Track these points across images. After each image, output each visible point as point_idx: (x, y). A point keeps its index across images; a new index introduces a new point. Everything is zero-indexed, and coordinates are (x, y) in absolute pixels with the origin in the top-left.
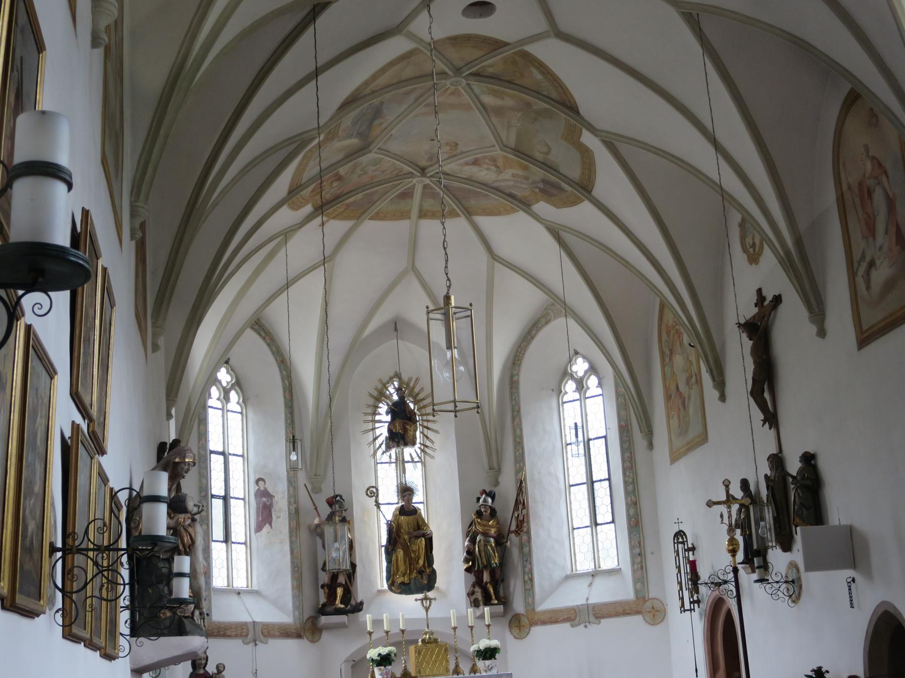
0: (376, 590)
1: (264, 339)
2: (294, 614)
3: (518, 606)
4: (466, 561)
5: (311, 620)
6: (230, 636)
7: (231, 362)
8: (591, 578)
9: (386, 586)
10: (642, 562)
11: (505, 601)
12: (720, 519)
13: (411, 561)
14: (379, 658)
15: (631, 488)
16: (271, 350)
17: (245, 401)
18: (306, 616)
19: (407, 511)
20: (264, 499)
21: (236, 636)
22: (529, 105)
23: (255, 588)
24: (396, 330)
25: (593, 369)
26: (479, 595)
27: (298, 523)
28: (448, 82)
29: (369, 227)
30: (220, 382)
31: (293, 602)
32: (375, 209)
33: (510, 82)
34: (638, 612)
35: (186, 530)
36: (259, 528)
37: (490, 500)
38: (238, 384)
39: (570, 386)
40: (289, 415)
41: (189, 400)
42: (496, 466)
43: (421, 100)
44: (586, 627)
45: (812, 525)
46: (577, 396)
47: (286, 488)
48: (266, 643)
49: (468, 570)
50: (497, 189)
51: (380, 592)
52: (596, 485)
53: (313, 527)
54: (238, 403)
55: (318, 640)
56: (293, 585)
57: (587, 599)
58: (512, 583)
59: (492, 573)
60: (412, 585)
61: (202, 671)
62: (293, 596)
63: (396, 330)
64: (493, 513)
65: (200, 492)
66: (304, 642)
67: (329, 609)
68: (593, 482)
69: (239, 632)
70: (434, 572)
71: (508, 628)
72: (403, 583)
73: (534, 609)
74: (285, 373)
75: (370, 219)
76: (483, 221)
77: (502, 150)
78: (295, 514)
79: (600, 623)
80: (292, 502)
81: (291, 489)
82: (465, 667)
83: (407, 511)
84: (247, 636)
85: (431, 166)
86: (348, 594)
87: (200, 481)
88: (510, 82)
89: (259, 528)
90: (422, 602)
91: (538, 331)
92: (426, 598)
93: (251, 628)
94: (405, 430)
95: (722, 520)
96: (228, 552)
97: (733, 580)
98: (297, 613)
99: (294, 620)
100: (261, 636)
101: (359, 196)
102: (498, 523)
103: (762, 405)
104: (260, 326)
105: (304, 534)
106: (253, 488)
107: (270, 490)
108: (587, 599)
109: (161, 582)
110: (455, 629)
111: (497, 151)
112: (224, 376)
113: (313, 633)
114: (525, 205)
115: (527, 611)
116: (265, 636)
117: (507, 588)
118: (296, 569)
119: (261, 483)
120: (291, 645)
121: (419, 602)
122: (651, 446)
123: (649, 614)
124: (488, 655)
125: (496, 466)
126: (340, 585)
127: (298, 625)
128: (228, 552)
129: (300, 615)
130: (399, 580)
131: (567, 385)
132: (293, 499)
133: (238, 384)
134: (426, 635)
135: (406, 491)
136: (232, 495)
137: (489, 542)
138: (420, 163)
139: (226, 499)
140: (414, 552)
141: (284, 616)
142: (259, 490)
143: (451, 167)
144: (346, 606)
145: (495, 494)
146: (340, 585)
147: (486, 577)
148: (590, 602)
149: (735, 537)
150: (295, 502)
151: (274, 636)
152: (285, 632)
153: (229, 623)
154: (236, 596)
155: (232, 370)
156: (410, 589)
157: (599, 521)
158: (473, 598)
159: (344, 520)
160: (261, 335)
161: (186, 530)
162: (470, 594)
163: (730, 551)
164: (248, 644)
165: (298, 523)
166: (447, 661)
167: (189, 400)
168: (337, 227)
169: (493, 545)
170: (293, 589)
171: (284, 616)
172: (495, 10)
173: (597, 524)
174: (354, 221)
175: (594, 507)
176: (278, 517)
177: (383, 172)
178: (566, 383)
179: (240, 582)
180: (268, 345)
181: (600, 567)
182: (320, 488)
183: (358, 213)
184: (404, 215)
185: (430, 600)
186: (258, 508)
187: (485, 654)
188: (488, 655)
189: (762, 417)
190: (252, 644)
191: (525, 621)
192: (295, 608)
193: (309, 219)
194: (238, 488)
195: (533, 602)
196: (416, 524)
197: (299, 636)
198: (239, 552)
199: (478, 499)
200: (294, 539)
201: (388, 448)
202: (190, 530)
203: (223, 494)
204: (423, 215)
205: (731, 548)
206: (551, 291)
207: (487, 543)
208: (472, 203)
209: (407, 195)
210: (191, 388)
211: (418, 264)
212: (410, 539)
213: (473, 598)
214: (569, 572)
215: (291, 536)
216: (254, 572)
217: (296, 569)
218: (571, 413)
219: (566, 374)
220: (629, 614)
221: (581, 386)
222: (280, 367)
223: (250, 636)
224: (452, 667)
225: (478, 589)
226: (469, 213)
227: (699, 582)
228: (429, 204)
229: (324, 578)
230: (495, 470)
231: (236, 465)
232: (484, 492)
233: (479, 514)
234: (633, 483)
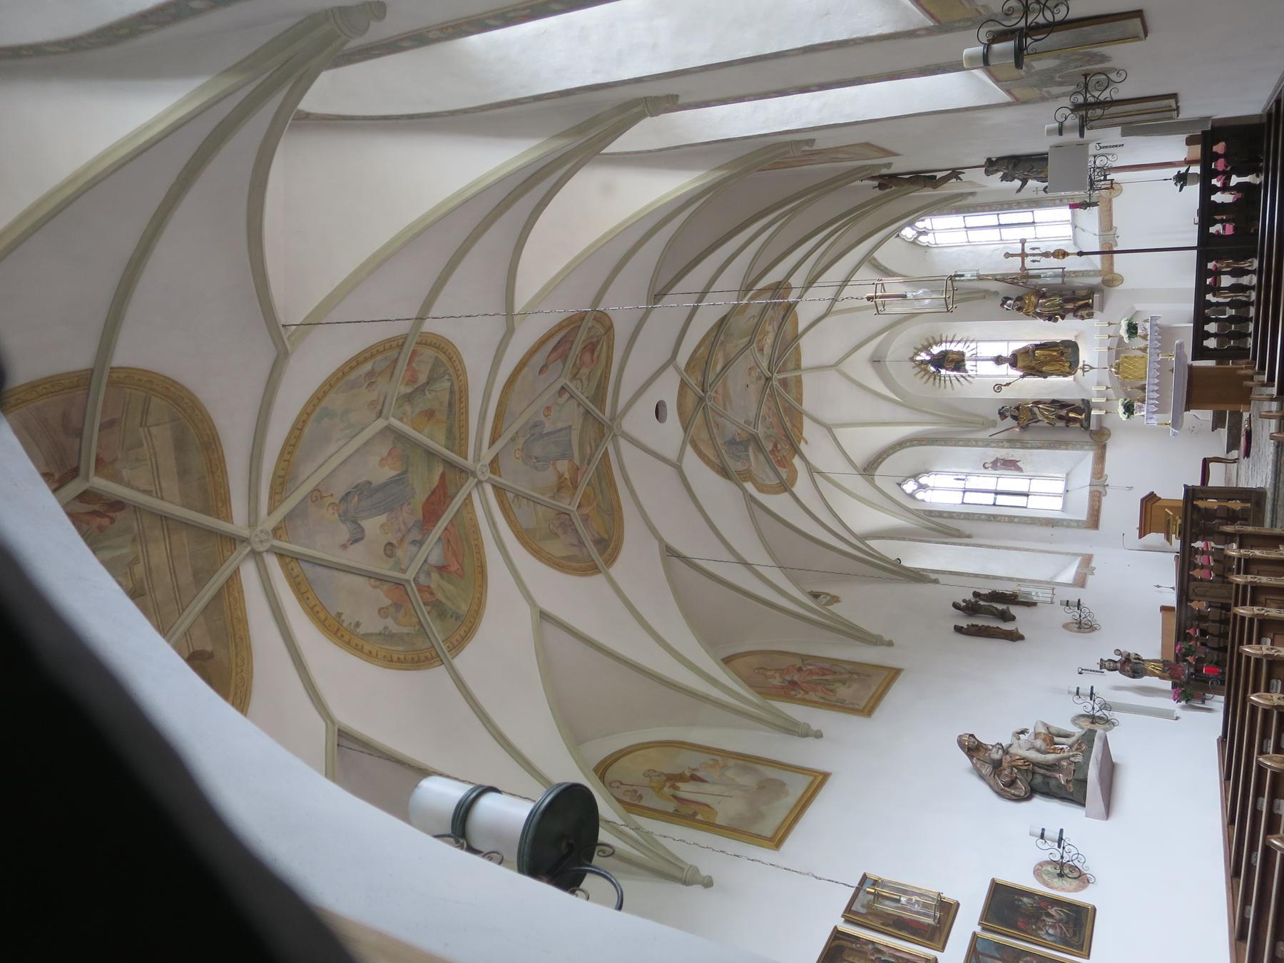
0: (1074, 383)
1: (884, 459)
2: (1086, 450)
3: (1096, 281)
4: (1056, 320)
5: (1092, 435)
6: (1099, 507)
7: (899, 482)
8: (1077, 229)
9: (1070, 378)
10: (1067, 199)
11: (1091, 291)
12: (1037, 263)
13: (1053, 360)
14: (1127, 414)
15: (1006, 206)
16: (892, 454)
17: (928, 472)
18: (1088, 439)
19: (1014, 361)
20: (999, 464)
21: (1100, 501)
22: (722, 343)
23: (1064, 476)
24: (879, 361)
25: (911, 224)
26: (1084, 313)
27: (1018, 441)
28: (709, 404)
29: (807, 405)
30: (914, 491)
31: (1077, 450)
32: (795, 404)
33: (707, 363)
34: (1110, 200)
35: (1014, 761)
36: (1020, 469)
37: (1009, 302)
38: (915, 477)
39: (923, 239)
40: (938, 443)
41: (927, 528)
42: (983, 294)
43: (721, 413)
44: (1118, 237)
45: (1047, 164)
46: (931, 235)
47: (991, 449)
48: (1107, 476)
49: (1063, 318)
50: (779, 328)
51: (1075, 380)
52: (1001, 223)
53: (1022, 430)
54: (925, 492)
55: (1109, 430)
56: (1064, 449)
57: (1095, 235)
58: (1076, 284)
59: (1067, 301)
60: (1072, 360)
61: (1119, 665)
62: (1073, 449)
63: (879, 361)
64: (1019, 299)
65: (991, 521)
66: (1110, 443)
67: (1085, 424)
68: (1000, 225)
69: (1096, 499)
70: (1063, 342)
71: (1114, 288)
72: (1070, 367)
73: (1100, 271)
74: (908, 444)
75: (801, 405)
76: (801, 328)
77: (753, 344)
78: (1013, 443)
79: (1107, 476)
80: (1001, 444)
81: (993, 445)
82: (1142, 343)
83: (1014, 361)
84: (1100, 493)
85: (764, 375)
86: (1077, 410)
87: (983, 520)
88: (707, 363)
89: (1020, 469)
90: (1086, 371)
91: (881, 265)
92: (1083, 369)
93: (1095, 488)
94: (953, 361)
95: (1038, 261)
96: (1035, 494)
97: (1091, 100)
98: (1086, 447)
99: (1092, 450)
100: (1102, 480)
101: (786, 419)
102: (1027, 294)
103: (945, 179)
104: (875, 462)
105: (1027, 436)
106: (990, 471)
107: (993, 460)
108: (1095, 235)
109: (1048, 784)
110: (1110, 324)
111: (754, 348)
112: (910, 487)
113: (1103, 435)
114: (790, 307)
115: (1101, 276)
116: (1101, 477)
117: (1081, 288)
118: (1052, 445)
119: (987, 465)
120: (1113, 454)
121: (1085, 374)
122: (972, 194)
123: (1112, 194)
124: (1134, 331)
125: (983, 294)
126: (1067, 414)
127: (1095, 447)
128: (1035, 494)
129: (1087, 445)
130: (1068, 370)
131: (923, 241)
132: (999, 444)
133: (915, 477)
134: (1111, 371)
135: (999, 360)
136: (994, 489)
137: (1042, 304)
138: (763, 384)
139: (997, 493)
140: (1046, 358)
141: (1087, 458)
142: (991, 467)
143: (765, 364)
144: (1084, 412)
145: (1004, 298)
146: (1067, 414)
147: (1070, 306)
148: (1097, 233)
149: (1052, 252)
150: (1002, 442)
151: (1103, 469)
152: (1100, 459)
153: (1089, 507)
154: (1069, 493)
155: (905, 480)
156: (1074, 362)
157: (1032, 221)
158: (1086, 317)
159: (1017, 408)
160: (882, 462)
161: (1014, 761)
162: (1082, 318)
163: (1064, 258)
164: (1106, 493)
165: (1018, 441)
166: (1135, 357)
167: (927, 528)
168: (808, 428)
169: (1044, 300)
170: (1067, 449)
171: (1088, 457)
172: (664, 402)
173: (1034, 223)
174: (804, 418)
175: (1019, 224)
176: (1013, 456)
177: (770, 409)
178: (920, 241)
179: (1059, 487)
180: (888, 456)
181: (1069, 221)
182: (992, 421)
183: (796, 414)
184: (799, 381)
185: (1084, 365)
186: (1005, 469)
187: (1133, 333)
188: (1134, 331)
189: (954, 180)
190: (1107, 488)
191: (1108, 277)
192: (1082, 448)
193: (803, 457)
194: (988, 482)
195: (1093, 271)
196: (1024, 355)
197: (1104, 447)
198: (1037, 485)
199: (1007, 309)
200: (1029, 446)
201: (966, 371)
202: (1014, 758)
203: (993, 495)
204: (798, 367)
205: (1061, 257)
206: (851, 272)
207: (1043, 305)
208: (789, 338)
209: (784, 383)
210: (916, 526)
211: (833, 362)
212: (1035, 360)
213: (1086, 317)
214: (1072, 242)
215: (1028, 448)
216: (1052, 475)
217: (1052, 445)
218: (942, 239)
219: (914, 243)
220: (1111, 208)
221: (924, 233)
222: (904, 448)
223: (1100, 489)
224: (1140, 353)
225: (1079, 313)
226: (797, 337)
227: (1088, 201)
228: (791, 365)
229: (1061, 424)
230: (986, 294)
231: (973, 482)
232: (1002, 305)
233: (1019, 309)
234: (1002, 205)
